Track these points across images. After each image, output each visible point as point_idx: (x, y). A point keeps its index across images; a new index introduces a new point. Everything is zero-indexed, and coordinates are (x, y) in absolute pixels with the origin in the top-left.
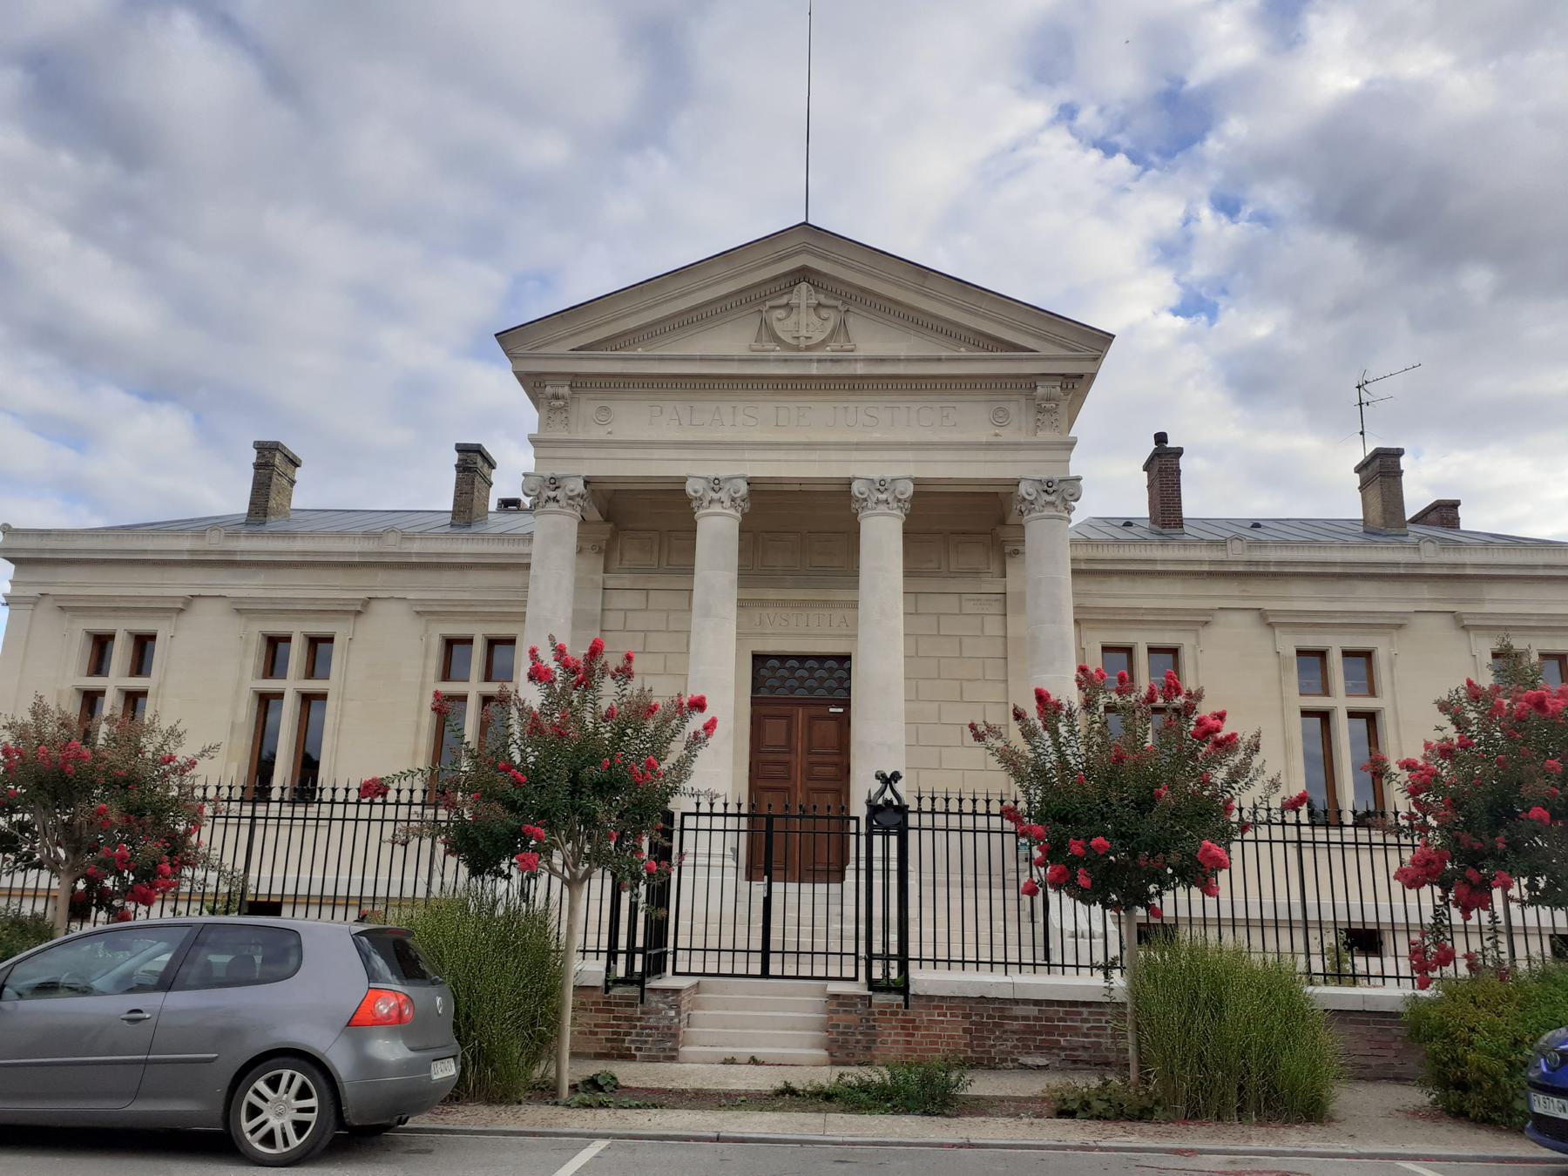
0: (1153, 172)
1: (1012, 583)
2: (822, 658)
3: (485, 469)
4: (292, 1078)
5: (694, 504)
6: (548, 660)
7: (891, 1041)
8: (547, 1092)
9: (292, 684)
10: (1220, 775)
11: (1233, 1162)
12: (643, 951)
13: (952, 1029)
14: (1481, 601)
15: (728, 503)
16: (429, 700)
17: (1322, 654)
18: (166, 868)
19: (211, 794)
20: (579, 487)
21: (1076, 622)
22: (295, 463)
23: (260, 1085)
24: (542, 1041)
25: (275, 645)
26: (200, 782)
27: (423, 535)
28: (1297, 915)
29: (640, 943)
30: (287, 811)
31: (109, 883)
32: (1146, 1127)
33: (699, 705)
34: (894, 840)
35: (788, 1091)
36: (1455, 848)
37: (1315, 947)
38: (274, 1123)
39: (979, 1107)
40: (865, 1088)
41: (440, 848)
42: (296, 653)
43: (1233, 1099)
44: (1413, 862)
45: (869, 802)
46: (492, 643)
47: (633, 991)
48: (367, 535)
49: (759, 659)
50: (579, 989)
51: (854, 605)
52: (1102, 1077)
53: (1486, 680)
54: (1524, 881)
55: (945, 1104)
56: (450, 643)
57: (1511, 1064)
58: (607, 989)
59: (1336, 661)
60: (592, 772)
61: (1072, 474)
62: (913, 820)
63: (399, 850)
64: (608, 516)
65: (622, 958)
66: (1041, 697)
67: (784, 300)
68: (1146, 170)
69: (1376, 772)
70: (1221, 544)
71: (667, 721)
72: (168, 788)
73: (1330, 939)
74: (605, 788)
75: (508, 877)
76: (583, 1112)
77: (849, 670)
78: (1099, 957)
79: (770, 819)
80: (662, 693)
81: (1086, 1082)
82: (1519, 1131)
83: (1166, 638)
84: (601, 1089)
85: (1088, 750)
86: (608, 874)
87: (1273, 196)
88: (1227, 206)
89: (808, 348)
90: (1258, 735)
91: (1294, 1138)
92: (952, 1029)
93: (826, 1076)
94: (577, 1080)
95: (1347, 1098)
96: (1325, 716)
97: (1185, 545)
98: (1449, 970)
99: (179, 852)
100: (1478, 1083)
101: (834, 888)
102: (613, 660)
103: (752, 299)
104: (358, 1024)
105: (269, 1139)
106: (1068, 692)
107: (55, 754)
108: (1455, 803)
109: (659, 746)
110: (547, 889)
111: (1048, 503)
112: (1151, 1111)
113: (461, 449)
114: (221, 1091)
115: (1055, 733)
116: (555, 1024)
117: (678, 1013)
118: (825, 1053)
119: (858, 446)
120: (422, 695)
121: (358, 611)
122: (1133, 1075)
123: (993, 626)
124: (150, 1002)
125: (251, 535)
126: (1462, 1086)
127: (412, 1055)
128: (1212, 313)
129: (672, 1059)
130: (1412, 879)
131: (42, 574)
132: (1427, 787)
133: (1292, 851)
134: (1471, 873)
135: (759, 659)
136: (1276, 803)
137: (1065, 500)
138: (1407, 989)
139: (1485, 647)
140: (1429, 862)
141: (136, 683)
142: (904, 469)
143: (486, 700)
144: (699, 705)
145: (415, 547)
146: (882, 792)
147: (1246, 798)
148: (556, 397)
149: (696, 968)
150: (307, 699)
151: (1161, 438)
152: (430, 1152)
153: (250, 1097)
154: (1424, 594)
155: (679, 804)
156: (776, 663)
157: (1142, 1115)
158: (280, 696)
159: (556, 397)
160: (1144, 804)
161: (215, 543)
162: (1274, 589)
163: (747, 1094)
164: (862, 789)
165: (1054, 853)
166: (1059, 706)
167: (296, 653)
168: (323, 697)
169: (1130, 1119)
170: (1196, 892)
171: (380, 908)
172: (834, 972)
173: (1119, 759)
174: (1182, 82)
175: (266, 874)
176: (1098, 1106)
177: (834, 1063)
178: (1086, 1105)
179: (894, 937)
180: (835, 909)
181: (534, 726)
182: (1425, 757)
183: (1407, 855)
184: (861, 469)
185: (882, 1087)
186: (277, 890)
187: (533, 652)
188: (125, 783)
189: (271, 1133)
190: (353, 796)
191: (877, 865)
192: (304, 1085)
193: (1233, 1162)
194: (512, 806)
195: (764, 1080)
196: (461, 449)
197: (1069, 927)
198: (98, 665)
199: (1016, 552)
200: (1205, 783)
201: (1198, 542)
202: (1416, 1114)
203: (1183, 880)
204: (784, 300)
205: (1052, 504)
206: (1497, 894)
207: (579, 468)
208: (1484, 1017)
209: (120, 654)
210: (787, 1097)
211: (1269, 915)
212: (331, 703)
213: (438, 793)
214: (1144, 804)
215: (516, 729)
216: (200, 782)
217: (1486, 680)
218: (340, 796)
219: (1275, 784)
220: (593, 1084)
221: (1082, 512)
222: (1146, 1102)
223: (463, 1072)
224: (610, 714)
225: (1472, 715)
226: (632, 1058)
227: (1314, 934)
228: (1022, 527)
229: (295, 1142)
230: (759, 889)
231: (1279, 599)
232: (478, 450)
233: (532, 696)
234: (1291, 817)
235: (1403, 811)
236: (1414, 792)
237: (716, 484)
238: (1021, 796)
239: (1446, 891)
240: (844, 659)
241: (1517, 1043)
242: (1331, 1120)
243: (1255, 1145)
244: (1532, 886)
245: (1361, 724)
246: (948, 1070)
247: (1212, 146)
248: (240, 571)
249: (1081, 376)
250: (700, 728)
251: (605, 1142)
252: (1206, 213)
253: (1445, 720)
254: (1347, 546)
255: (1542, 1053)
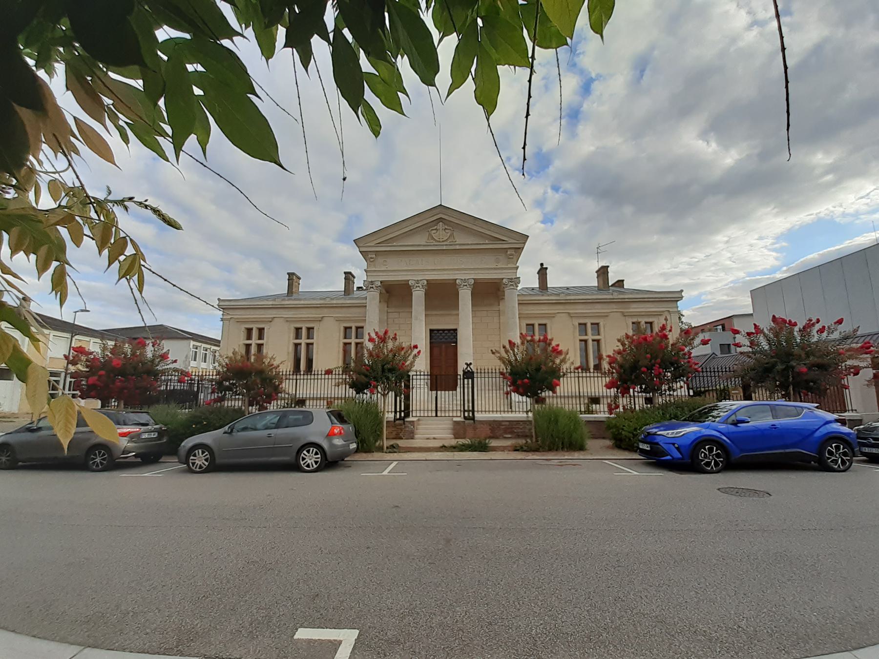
0: (534, 178)
1: (501, 307)
2: (449, 330)
3: (353, 279)
4: (313, 450)
5: (412, 287)
6: (373, 335)
7: (470, 432)
8: (380, 449)
9: (303, 341)
10: (558, 361)
11: (561, 462)
12: (404, 411)
13: (486, 430)
14: (629, 308)
15: (421, 287)
16: (341, 345)
17: (585, 324)
18: (274, 394)
19: (284, 373)
20: (379, 284)
21: (519, 318)
22: (299, 278)
23: (305, 452)
24: (379, 436)
25: (298, 330)
26: (281, 370)
27: (337, 299)
28: (577, 394)
29: (403, 409)
30: (306, 377)
31: (259, 398)
32: (537, 453)
33: (416, 347)
34: (470, 380)
35: (444, 446)
36: (620, 378)
37: (582, 402)
38: (309, 462)
39: (494, 449)
40: (463, 445)
41: (348, 386)
42: (304, 332)
43: (560, 446)
44: (609, 382)
45: (463, 371)
46: (357, 328)
47: (401, 422)
48: (321, 299)
49: (431, 331)
50: (388, 422)
51: (458, 315)
52: (526, 440)
53: (631, 333)
54: (639, 387)
55: (485, 449)
56: (346, 328)
57: (633, 434)
58: (395, 421)
59: (589, 326)
60: (388, 366)
61: (518, 276)
62: (475, 375)
63: (337, 388)
64: (387, 292)
65: (398, 414)
66: (510, 342)
67: (435, 228)
68: (532, 177)
69: (600, 358)
70: (558, 295)
71: (407, 351)
72: (272, 372)
73: (586, 401)
74: (391, 370)
75: (367, 394)
76: (390, 454)
77: (457, 333)
78: (525, 410)
79: (436, 376)
80: (405, 343)
81: (522, 442)
82: (636, 451)
83: (543, 322)
84: (394, 448)
85: (523, 355)
86: (393, 393)
87: (568, 185)
88: (555, 188)
89: (443, 241)
90: (568, 350)
91: (576, 455)
92: (487, 430)
93: (454, 442)
94: (388, 445)
95: (590, 443)
96: (586, 341)
97: (548, 295)
98: (618, 410)
99: (277, 390)
100: (625, 440)
101: (454, 392)
102: (391, 334)
103: (426, 227)
104: (331, 435)
105: (308, 466)
106: (518, 341)
107: (240, 364)
108: (621, 366)
109: (405, 359)
110: (377, 397)
111: (511, 285)
112: (539, 449)
113: (345, 273)
114: (295, 454)
115: (514, 351)
116: (382, 432)
117: (414, 427)
118: (452, 436)
119: (458, 269)
120: (339, 343)
121: (321, 320)
122: (534, 440)
123: (496, 320)
124: (273, 432)
125: (289, 300)
126: (621, 440)
127: (344, 443)
128: (552, 222)
129: (412, 439)
130: (609, 386)
131: (230, 312)
132: (614, 363)
133: (577, 379)
134: (625, 385)
135: (431, 331)
136: (572, 368)
137: (516, 284)
138: (607, 415)
139: (630, 321)
140: (613, 382)
141: (260, 342)
142: (471, 276)
143: (357, 344)
144: (416, 347)
145: (335, 302)
146: (467, 368)
147: (565, 367)
148: (371, 258)
149: (418, 415)
150: (308, 345)
151: (542, 265)
152: (350, 467)
153: (302, 455)
154: (614, 308)
155: (411, 374)
156: (436, 332)
157: (536, 450)
158: (300, 344)
159: (371, 258)
160: (538, 369)
161: (278, 302)
162: (572, 307)
163: (433, 447)
164: (461, 367)
165: (513, 383)
166: (514, 344)
167: (304, 332)
168: (312, 344)
169: (534, 451)
170: (550, 392)
171: (333, 400)
172: (455, 415)
173: (531, 358)
174: (541, 150)
175: (301, 392)
176: (525, 448)
177: (456, 438)
178: (522, 448)
179: (471, 405)
180: (454, 397)
181: (371, 354)
182: (613, 354)
183: (608, 379)
184: (459, 276)
185: (468, 445)
186: (304, 396)
187: (369, 334)
188: (260, 372)
189: (309, 464)
190: (323, 373)
191: (466, 386)
192: (316, 452)
193: (561, 462)
194: (366, 376)
195: (438, 444)
196: (345, 273)
197: (517, 400)
198: (249, 337)
199: (503, 299)
200: (554, 363)
201: (552, 294)
202: (608, 447)
203: (547, 389)
204: (435, 228)
205: (512, 285)
206: (631, 390)
207: (379, 278)
208: (627, 423)
209: (255, 334)
210: (443, 448)
211: (570, 394)
212: (315, 345)
213: (346, 369)
214: (538, 369)
215: (366, 355)
216: (281, 370)
217: (631, 333)
218: (320, 373)
219: (572, 363)
220: (392, 446)
221: (520, 287)
222: (538, 447)
223: (358, 446)
224: (391, 350)
225: (627, 343)
226: (402, 439)
227: (582, 399)
228: (504, 291)
229: (315, 466)
230: (434, 392)
231: (572, 310)
232: (350, 273)
233: (370, 346)
234: (576, 371)
235: (607, 369)
236: (610, 364)
237: (418, 282)
238: (504, 368)
239: (618, 389)
240: (455, 330)
241: (635, 429)
242: (586, 450)
243: (566, 457)
244: (641, 388)
245: (596, 343)
246: (485, 440)
247: (551, 169)
248: (287, 310)
249: (519, 248)
250: (416, 353)
251: (397, 462)
252: (549, 191)
253: (619, 344)
254: (593, 294)
255: (643, 432)
